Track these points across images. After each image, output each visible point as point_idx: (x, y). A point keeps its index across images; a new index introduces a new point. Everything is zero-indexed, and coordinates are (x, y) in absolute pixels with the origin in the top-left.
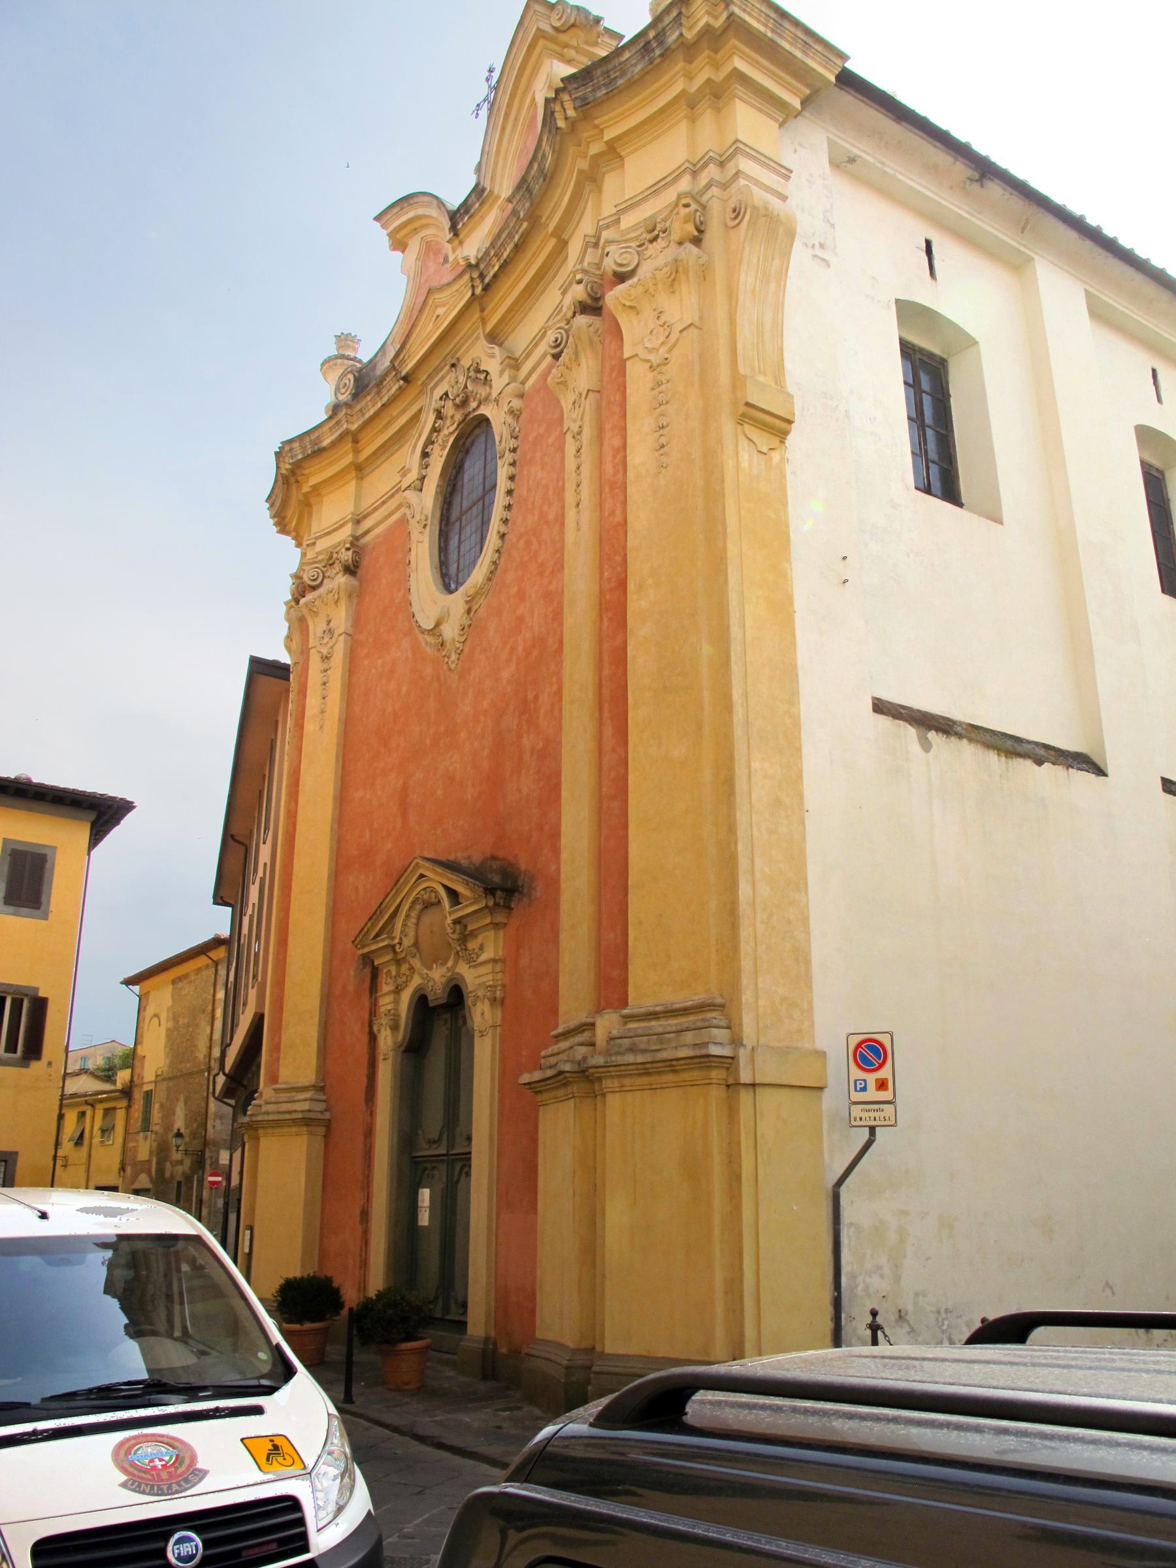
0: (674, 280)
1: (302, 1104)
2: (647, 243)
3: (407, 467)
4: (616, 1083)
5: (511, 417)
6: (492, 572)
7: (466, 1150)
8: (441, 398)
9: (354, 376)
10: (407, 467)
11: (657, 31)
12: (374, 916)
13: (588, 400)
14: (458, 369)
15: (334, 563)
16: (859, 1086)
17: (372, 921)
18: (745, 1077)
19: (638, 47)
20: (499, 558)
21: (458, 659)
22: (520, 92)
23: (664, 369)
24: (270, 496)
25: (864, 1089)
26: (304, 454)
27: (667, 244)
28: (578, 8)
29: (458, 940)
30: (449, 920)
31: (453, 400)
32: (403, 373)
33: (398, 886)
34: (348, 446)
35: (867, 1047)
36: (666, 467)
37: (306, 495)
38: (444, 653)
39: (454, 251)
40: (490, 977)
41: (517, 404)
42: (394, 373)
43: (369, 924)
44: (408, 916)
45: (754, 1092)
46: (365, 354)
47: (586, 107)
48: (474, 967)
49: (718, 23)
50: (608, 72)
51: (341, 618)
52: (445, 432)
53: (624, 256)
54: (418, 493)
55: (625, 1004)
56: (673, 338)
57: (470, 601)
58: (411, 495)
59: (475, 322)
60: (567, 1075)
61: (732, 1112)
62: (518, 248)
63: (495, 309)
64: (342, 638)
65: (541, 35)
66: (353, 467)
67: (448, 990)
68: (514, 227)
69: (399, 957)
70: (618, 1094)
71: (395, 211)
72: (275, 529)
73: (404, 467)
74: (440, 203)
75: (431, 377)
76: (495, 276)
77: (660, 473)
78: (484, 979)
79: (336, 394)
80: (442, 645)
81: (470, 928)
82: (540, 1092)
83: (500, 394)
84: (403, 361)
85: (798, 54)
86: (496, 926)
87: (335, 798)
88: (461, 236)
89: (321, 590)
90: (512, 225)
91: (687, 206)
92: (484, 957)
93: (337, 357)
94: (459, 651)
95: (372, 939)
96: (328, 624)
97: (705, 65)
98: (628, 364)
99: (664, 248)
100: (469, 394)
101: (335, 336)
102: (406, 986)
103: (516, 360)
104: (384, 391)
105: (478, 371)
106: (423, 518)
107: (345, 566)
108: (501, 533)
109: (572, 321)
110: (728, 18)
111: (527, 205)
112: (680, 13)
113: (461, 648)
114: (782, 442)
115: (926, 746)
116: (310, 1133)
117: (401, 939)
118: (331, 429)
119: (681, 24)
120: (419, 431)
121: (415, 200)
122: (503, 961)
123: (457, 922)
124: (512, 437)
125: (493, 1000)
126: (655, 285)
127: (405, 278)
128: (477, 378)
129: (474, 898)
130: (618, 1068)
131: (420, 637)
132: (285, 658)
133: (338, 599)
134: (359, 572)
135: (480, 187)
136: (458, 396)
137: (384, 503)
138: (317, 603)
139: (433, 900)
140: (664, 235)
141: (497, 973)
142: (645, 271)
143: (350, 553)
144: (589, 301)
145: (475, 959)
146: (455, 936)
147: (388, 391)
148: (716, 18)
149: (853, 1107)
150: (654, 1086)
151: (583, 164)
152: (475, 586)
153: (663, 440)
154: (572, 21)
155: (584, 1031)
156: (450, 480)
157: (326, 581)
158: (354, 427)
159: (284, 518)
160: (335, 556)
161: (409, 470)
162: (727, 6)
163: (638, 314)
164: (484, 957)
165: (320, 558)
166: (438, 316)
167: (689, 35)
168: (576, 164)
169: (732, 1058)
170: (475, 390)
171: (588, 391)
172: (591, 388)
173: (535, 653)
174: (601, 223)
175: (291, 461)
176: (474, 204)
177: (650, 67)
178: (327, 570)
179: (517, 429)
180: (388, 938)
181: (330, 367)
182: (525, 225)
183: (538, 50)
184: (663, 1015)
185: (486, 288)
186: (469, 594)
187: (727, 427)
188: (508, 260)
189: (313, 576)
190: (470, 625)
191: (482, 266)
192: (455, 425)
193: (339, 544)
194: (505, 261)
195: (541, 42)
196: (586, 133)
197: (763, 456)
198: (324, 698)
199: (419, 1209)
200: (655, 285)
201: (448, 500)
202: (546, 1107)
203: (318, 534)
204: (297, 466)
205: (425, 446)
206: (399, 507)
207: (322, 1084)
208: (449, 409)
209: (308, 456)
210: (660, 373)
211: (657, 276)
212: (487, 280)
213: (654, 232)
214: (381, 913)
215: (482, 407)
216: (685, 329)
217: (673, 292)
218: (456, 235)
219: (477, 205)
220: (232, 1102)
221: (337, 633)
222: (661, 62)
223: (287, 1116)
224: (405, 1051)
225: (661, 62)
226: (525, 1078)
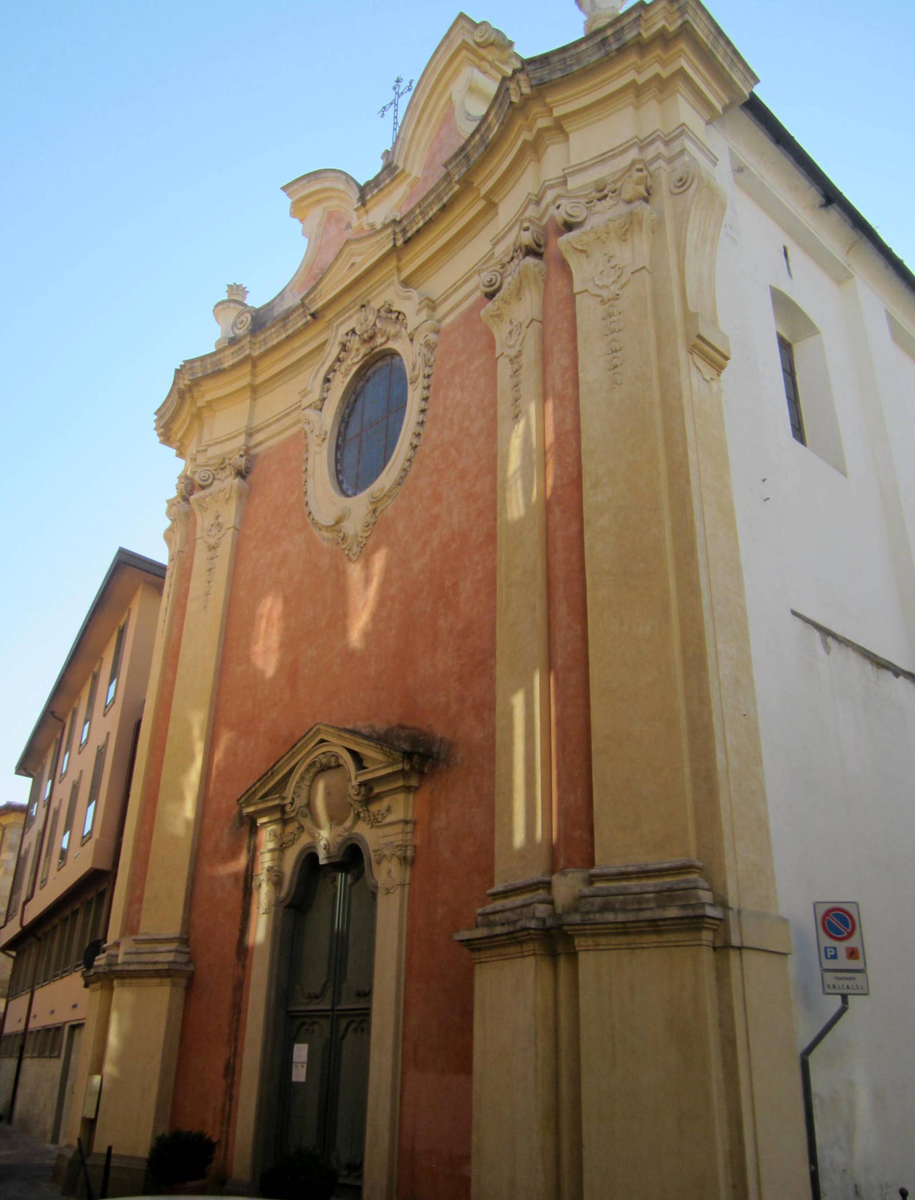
0: (627, 230)
1: (165, 956)
2: (595, 201)
3: (308, 389)
4: (590, 942)
5: (427, 349)
6: (402, 478)
7: (366, 1006)
8: (347, 334)
9: (252, 315)
10: (308, 389)
11: (614, 30)
12: (264, 778)
13: (530, 328)
14: (368, 310)
15: (225, 468)
16: (829, 954)
17: (261, 782)
18: (735, 940)
19: (595, 41)
20: (410, 466)
21: (361, 552)
22: (438, 91)
23: (615, 303)
24: (159, 410)
25: (835, 957)
26: (204, 373)
27: (615, 203)
28: (498, 32)
29: (360, 802)
30: (355, 783)
31: (360, 336)
32: (313, 310)
33: (295, 749)
34: (247, 368)
35: (836, 915)
36: (620, 384)
37: (200, 409)
38: (344, 547)
39: (359, 218)
40: (400, 837)
41: (432, 337)
42: (302, 310)
43: (258, 785)
44: (302, 778)
45: (741, 955)
46: (256, 300)
47: (542, 87)
48: (378, 827)
49: (672, 28)
50: (565, 59)
51: (230, 514)
52: (349, 362)
53: (575, 209)
54: (318, 412)
55: (592, 864)
56: (624, 279)
57: (376, 503)
58: (311, 414)
59: (391, 270)
60: (532, 932)
61: (722, 976)
62: (444, 209)
63: (411, 261)
64: (231, 531)
65: (464, 46)
66: (249, 389)
67: (343, 849)
68: (444, 190)
69: (287, 817)
70: (591, 953)
71: (302, 183)
72: (158, 439)
73: (306, 389)
74: (349, 179)
75: (338, 315)
76: (418, 231)
77: (614, 389)
78: (392, 839)
79: (232, 329)
80: (342, 540)
81: (377, 790)
82: (479, 950)
83: (416, 329)
84: (313, 301)
85: (727, 68)
86: (408, 789)
87: (216, 670)
88: (368, 206)
89: (212, 489)
90: (441, 188)
91: (640, 170)
92: (390, 818)
93: (230, 301)
94: (362, 545)
95: (259, 799)
96: (217, 519)
97: (654, 63)
98: (578, 298)
99: (612, 206)
100: (377, 331)
101: (228, 285)
102: (292, 844)
103: (433, 302)
104: (289, 327)
105: (391, 311)
106: (323, 433)
107: (238, 470)
108: (414, 445)
109: (507, 266)
110: (682, 25)
111: (464, 170)
112: (640, 16)
113: (364, 542)
114: (718, 375)
115: (827, 649)
116: (174, 985)
117: (293, 799)
118: (233, 353)
119: (640, 25)
120: (323, 359)
121: (323, 175)
122: (415, 823)
123: (361, 784)
124: (426, 365)
125: (404, 860)
126: (608, 233)
127: (307, 240)
128: (387, 318)
129: (388, 762)
130: (596, 927)
131: (317, 533)
132: (160, 553)
133: (229, 497)
134: (249, 478)
135: (393, 166)
136: (367, 332)
137: (278, 420)
138: (207, 500)
139: (333, 764)
140: (613, 195)
141: (407, 833)
142: (595, 222)
143: (244, 459)
144: (534, 246)
145: (380, 820)
146: (359, 798)
147: (294, 325)
148: (671, 24)
149: (827, 975)
150: (632, 946)
151: (527, 136)
152: (382, 489)
153: (615, 361)
154: (492, 39)
155: (538, 889)
156: (349, 403)
157: (215, 483)
158: (256, 354)
159: (170, 430)
160: (227, 461)
161: (310, 392)
162: (682, 15)
163: (588, 257)
164: (390, 818)
165: (211, 462)
166: (353, 264)
167: (646, 35)
168: (522, 136)
169: (720, 920)
170: (384, 328)
171: (532, 320)
172: (535, 318)
173: (454, 546)
174: (547, 183)
175: (191, 378)
176: (385, 180)
177: (606, 58)
178: (218, 473)
179: (432, 359)
180: (279, 798)
181: (224, 309)
182: (457, 188)
183: (459, 59)
184: (635, 876)
185: (406, 242)
186: (375, 495)
187: (682, 354)
188: (433, 219)
189: (205, 477)
190: (374, 523)
191: (405, 223)
192: (360, 357)
193: (232, 452)
194: (431, 219)
195: (464, 53)
196: (536, 109)
197: (705, 382)
198: (209, 582)
199: (294, 1065)
200: (608, 233)
201: (347, 419)
202: (484, 965)
203: (209, 443)
204: (196, 383)
205: (328, 373)
206: (298, 422)
207: (186, 937)
208: (355, 342)
209: (208, 375)
210: (611, 306)
211: (610, 226)
212: (409, 234)
213: (602, 192)
214: (272, 774)
215: (390, 342)
216: (637, 271)
217: (625, 240)
218: (364, 205)
219: (388, 181)
220: (14, 954)
221: (225, 527)
222: (616, 55)
223: (150, 967)
224: (287, 907)
225: (616, 55)
226: (464, 935)
